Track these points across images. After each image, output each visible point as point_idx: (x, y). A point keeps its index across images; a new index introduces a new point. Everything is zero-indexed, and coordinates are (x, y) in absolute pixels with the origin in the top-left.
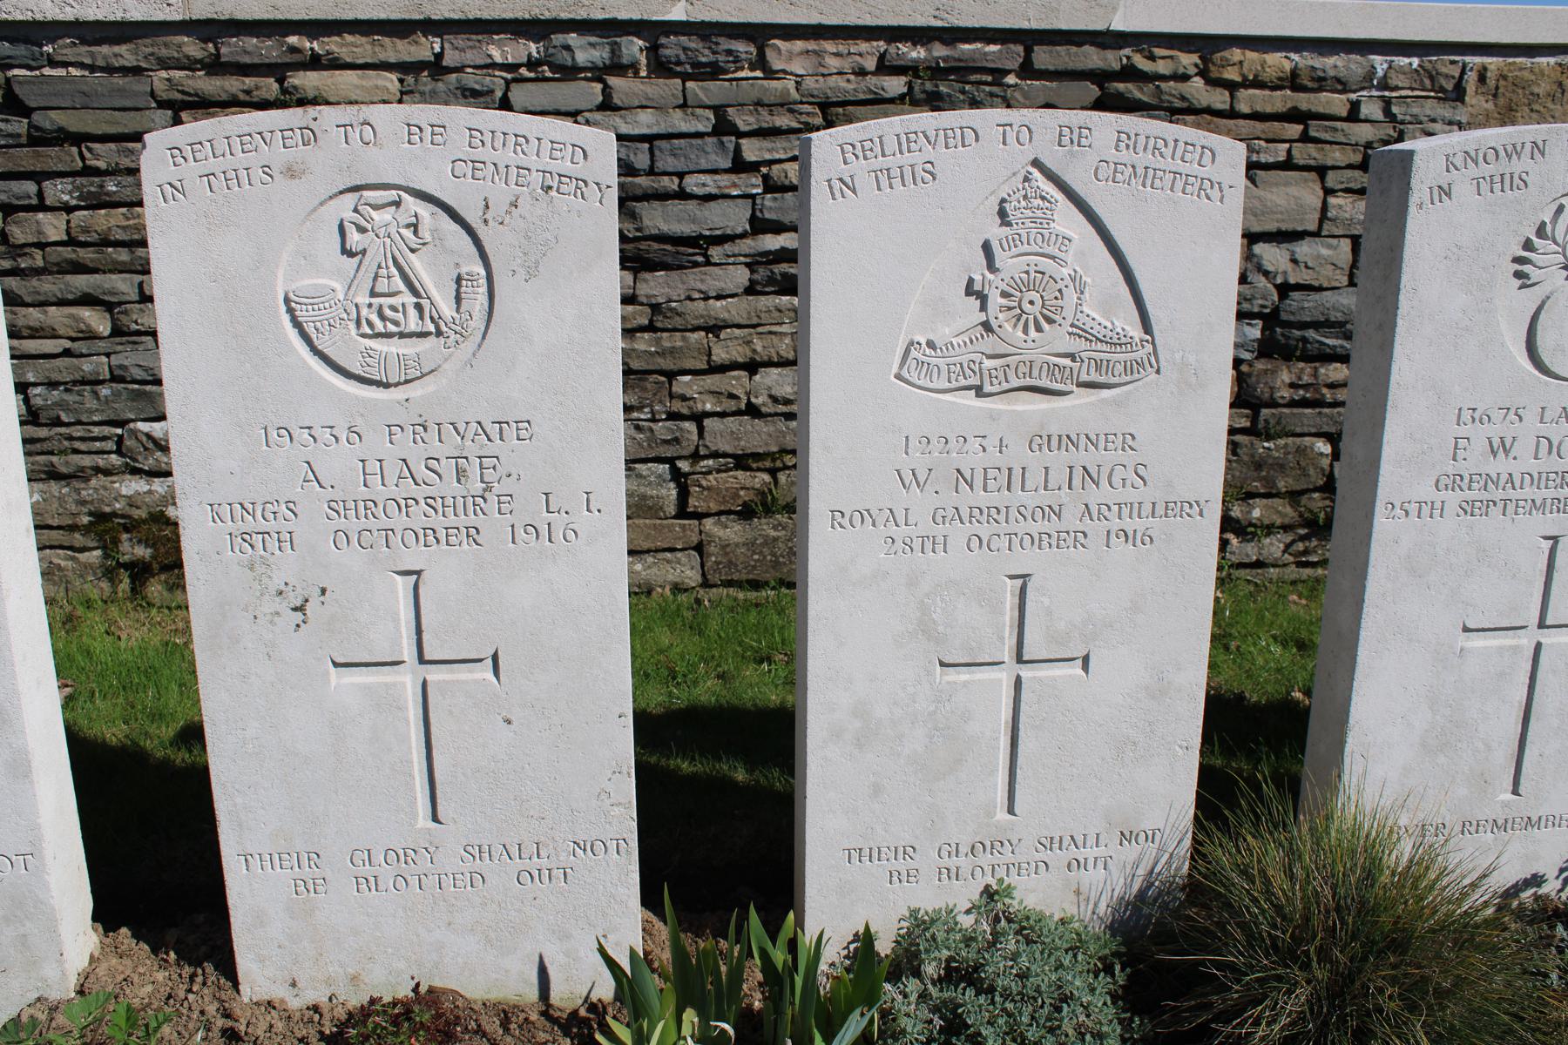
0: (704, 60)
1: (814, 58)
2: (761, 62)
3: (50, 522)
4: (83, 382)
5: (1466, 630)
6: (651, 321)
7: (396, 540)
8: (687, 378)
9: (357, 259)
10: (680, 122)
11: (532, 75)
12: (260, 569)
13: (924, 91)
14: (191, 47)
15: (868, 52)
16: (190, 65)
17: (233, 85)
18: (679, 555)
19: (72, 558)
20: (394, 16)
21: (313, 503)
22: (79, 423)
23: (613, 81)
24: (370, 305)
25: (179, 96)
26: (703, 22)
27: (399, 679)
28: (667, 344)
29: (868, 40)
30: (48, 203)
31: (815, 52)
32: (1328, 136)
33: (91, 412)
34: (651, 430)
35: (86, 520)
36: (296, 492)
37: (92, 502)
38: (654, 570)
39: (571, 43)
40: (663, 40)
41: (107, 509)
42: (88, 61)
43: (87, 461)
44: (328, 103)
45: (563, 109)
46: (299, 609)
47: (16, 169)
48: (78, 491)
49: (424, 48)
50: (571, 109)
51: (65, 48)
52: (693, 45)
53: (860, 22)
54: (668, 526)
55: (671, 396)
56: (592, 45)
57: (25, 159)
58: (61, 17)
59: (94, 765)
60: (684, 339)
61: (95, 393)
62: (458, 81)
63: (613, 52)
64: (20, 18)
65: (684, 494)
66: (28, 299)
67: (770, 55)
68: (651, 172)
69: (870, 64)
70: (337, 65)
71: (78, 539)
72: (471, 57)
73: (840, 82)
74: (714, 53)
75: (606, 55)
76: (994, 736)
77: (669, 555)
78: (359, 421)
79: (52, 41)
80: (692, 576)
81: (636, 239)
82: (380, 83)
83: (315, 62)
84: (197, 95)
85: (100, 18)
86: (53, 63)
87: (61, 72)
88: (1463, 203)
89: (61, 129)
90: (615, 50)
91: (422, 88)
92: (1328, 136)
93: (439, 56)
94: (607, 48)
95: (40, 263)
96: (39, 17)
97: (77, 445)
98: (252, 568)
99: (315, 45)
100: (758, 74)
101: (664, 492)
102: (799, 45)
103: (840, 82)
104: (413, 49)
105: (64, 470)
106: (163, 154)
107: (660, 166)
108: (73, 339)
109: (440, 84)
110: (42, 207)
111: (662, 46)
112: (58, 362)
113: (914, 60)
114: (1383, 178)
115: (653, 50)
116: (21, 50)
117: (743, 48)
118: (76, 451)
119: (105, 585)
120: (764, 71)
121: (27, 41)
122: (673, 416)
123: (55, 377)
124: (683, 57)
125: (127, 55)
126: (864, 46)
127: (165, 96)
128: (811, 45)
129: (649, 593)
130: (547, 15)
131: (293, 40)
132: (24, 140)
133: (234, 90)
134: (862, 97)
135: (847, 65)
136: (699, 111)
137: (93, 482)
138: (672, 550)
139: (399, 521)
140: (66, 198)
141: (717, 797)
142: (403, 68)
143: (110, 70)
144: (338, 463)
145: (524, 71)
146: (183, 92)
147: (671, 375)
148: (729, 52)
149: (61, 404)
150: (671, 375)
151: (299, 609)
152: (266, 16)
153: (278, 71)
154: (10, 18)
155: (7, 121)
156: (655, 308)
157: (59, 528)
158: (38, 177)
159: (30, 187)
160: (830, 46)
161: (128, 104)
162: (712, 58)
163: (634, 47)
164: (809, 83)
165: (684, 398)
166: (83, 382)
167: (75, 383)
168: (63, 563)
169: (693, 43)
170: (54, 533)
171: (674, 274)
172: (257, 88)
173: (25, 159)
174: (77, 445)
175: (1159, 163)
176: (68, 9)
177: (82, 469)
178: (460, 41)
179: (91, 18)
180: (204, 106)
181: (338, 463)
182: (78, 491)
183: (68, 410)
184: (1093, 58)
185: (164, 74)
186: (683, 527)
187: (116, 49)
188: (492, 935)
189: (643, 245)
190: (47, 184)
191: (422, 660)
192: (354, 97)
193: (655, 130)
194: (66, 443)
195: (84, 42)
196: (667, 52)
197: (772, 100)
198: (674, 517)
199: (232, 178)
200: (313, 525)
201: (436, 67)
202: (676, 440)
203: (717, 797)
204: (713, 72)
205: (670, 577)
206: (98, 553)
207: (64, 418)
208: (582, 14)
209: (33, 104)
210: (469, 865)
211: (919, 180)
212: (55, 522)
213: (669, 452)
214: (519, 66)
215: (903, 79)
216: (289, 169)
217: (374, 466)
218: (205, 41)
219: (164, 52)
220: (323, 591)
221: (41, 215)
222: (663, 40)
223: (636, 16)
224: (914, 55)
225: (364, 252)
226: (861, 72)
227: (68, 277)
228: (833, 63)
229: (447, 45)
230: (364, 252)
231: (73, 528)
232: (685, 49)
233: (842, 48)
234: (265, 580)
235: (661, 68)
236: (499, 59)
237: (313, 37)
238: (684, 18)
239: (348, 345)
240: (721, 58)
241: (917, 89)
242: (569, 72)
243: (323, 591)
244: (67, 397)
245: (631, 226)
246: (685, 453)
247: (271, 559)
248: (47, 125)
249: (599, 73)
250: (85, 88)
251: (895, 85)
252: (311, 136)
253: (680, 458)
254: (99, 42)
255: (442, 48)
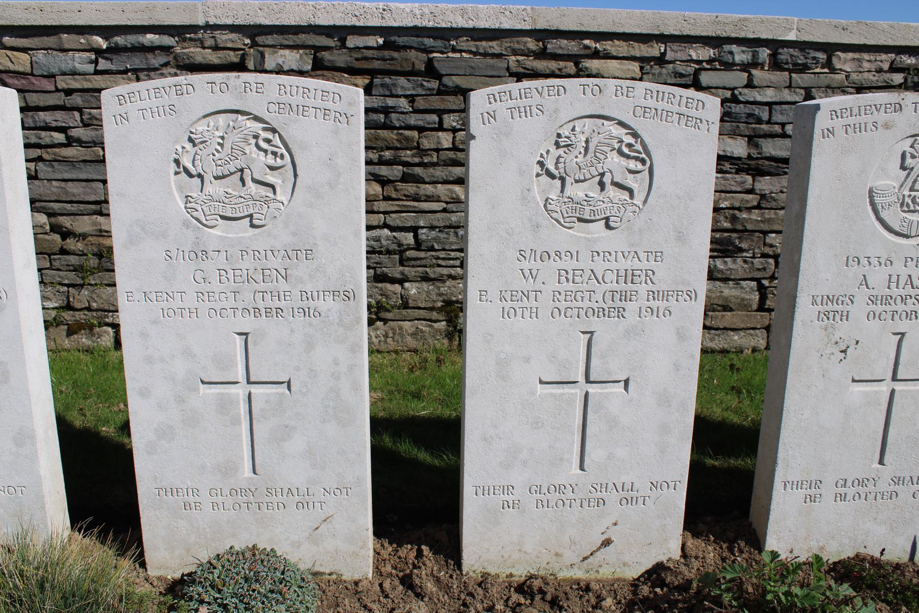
0: (800, 62)
1: (856, 63)
2: (829, 64)
3: (420, 305)
4: (450, 227)
5: (854, 381)
6: (759, 203)
7: (896, 317)
8: (774, 235)
9: (906, 172)
10: (787, 96)
11: (709, 67)
12: (830, 330)
13: (913, 82)
14: (531, 44)
15: (885, 60)
16: (527, 53)
17: (553, 65)
18: (757, 331)
19: (430, 326)
20: (644, 32)
21: (862, 296)
22: (444, 250)
23: (754, 72)
24: (910, 196)
25: (522, 70)
26: (804, 42)
27: (573, 391)
28: (767, 216)
29: (886, 53)
30: (445, 126)
31: (858, 60)
32: (766, 104)
33: (452, 244)
34: (752, 263)
35: (440, 304)
36: (854, 291)
37: (446, 295)
38: (744, 339)
39: (733, 50)
40: (780, 51)
41: (454, 299)
42: (474, 50)
43: (445, 271)
44: (603, 77)
45: (728, 86)
46: (844, 351)
47: (430, 108)
48: (439, 288)
49: (655, 50)
50: (732, 86)
51: (463, 43)
52: (796, 54)
53: (886, 43)
54: (754, 316)
55: (765, 244)
56: (743, 52)
57: (436, 102)
58: (466, 26)
59: (709, 434)
60: (776, 214)
61: (456, 233)
62: (674, 68)
63: (753, 56)
64: (444, 26)
65: (763, 298)
66: (427, 180)
67: (835, 60)
68: (769, 122)
69: (886, 66)
70: (608, 56)
71: (435, 315)
72: (681, 56)
73: (870, 76)
74: (806, 58)
75: (749, 58)
76: (574, 445)
77: (752, 331)
78: (893, 255)
79: (456, 38)
80: (762, 343)
81: (758, 159)
82: (630, 67)
83: (596, 55)
84: (532, 70)
85: (487, 27)
86: (454, 50)
87: (458, 55)
88: (853, 150)
89: (457, 87)
90: (755, 55)
91: (653, 71)
92: (766, 104)
93: (663, 54)
94: (751, 54)
95: (435, 160)
96: (454, 26)
97: (440, 262)
98: (826, 330)
99: (598, 45)
100: (826, 70)
101: (753, 297)
102: (850, 55)
103: (870, 76)
104: (649, 50)
105: (432, 276)
106: (479, 99)
107: (774, 119)
108: (447, 203)
109: (664, 70)
110: (441, 128)
111: (780, 54)
112: (438, 215)
113: (909, 65)
114: (84, 104)
115: (774, 56)
116: (439, 43)
117: (822, 56)
118: (439, 266)
119: (446, 341)
120: (829, 69)
121: (442, 38)
122: (764, 256)
123: (436, 223)
124: (790, 60)
125: (496, 47)
126: (884, 57)
127: (514, 70)
128: (857, 56)
129: (742, 352)
130: (725, 35)
131: (587, 42)
132: (435, 92)
133: (553, 68)
134: (880, 84)
135: (873, 67)
136: (798, 90)
137: (448, 283)
138: (754, 329)
139: (900, 307)
140: (454, 124)
141: (416, 477)
142: (642, 60)
143: (485, 55)
144: (878, 277)
145: (704, 64)
146: (525, 68)
147: (765, 233)
148: (814, 58)
149: (436, 239)
150: (765, 233)
151: (844, 351)
152: (576, 29)
153: (576, 59)
154: (439, 26)
155: (428, 81)
156: (763, 196)
157: (424, 308)
158: (440, 113)
159: (435, 118)
160: (866, 56)
161: (495, 73)
162: (804, 61)
163: (764, 54)
164: (854, 76)
165: (771, 246)
166: (450, 227)
167: (445, 227)
168: (424, 329)
169: (795, 52)
170: (421, 311)
171: (775, 179)
172: (566, 67)
173: (436, 102)
174: (440, 262)
175: (669, 107)
176: (470, 22)
177: (442, 276)
178: (675, 46)
179: (482, 27)
180: (535, 75)
181: (878, 277)
182: (439, 288)
183: (439, 242)
184: (571, 46)
185: (513, 58)
186: (762, 316)
187: (490, 43)
188: (894, 525)
189: (760, 162)
190: (445, 116)
191: (249, 382)
192: (617, 75)
193: (774, 100)
194: (434, 261)
195: (474, 39)
196: (782, 57)
197: (835, 85)
198: (756, 311)
199: (859, 128)
200: (859, 310)
201: (661, 60)
202: (764, 269)
203: (416, 477)
204: (803, 69)
205: (752, 344)
206: (444, 323)
207: (436, 247)
208: (742, 35)
209: (444, 73)
210: (892, 488)
211: (534, 114)
212: (423, 305)
213: (758, 275)
214: (701, 62)
215: (902, 75)
216: (886, 124)
217: (894, 279)
218: (538, 41)
219: (517, 46)
220: (857, 342)
221: (440, 133)
222: (780, 51)
223: (770, 37)
224: (909, 61)
225: (912, 168)
226: (880, 71)
227: (450, 168)
228: (866, 65)
229: (668, 49)
230: (912, 168)
231: (432, 309)
232: (792, 56)
233: (873, 58)
234: (831, 336)
235: (776, 65)
236: (695, 58)
237: (597, 41)
238: (795, 39)
239: (894, 216)
240: (809, 61)
241: (909, 80)
242: (728, 66)
243: (857, 342)
244: (440, 235)
245: (755, 152)
246: (767, 276)
247: (837, 325)
248: (450, 84)
249: (745, 67)
250: (473, 64)
251: (898, 78)
252: (899, 108)
253: (765, 278)
254: (480, 40)
255: (665, 50)
